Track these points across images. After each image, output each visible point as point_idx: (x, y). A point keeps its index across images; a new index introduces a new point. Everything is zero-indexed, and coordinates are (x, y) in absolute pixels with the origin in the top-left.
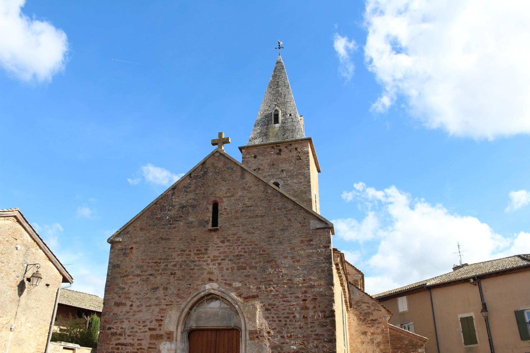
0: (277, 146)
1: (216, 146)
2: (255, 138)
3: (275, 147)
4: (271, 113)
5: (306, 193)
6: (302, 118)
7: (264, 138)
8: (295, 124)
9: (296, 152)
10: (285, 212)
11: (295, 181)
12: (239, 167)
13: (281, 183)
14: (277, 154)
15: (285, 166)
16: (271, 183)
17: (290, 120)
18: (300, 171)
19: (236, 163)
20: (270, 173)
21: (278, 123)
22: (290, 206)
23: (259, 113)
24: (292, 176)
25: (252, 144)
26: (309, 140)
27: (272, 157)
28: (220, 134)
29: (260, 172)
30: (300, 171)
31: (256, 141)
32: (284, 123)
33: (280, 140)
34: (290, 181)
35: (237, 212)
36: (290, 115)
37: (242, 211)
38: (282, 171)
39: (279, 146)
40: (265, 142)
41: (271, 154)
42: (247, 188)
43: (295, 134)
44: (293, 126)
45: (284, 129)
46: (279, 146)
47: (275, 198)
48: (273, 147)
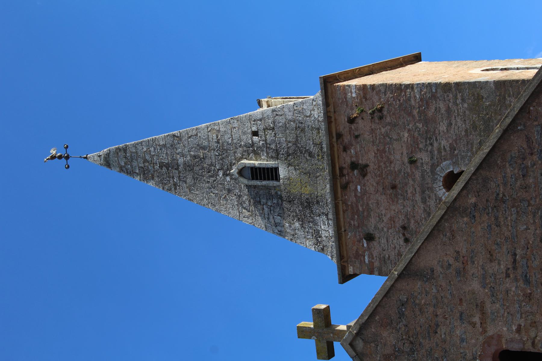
0: (342, 175)
1: (337, 346)
2: (317, 235)
3: (344, 180)
4: (248, 187)
5: (479, 98)
6: (264, 101)
7: (316, 209)
8: (281, 120)
9: (360, 121)
10: (535, 157)
11: (443, 127)
12: (399, 286)
13: (447, 167)
14: (364, 175)
15: (399, 155)
16: (446, 196)
17: (270, 136)
18: (415, 112)
19: (387, 294)
20: (418, 198)
21: (276, 169)
22: (518, 143)
23: (248, 221)
24: (429, 136)
25: (331, 244)
26: (327, 83)
27: (372, 189)
28: (303, 333)
29: (412, 225)
30: (415, 112)
31: (324, 234)
32: (277, 152)
33: (325, 165)
34: (444, 143)
35: (529, 297)
36: (255, 134)
37: (527, 281)
38: (412, 162)
39: (341, 169)
40: (329, 209)
41: (364, 192)
42: (459, 265)
43: (309, 122)
44: (285, 127)
45: (294, 153)
46: (341, 169)
47: (493, 185)
48: (345, 187)
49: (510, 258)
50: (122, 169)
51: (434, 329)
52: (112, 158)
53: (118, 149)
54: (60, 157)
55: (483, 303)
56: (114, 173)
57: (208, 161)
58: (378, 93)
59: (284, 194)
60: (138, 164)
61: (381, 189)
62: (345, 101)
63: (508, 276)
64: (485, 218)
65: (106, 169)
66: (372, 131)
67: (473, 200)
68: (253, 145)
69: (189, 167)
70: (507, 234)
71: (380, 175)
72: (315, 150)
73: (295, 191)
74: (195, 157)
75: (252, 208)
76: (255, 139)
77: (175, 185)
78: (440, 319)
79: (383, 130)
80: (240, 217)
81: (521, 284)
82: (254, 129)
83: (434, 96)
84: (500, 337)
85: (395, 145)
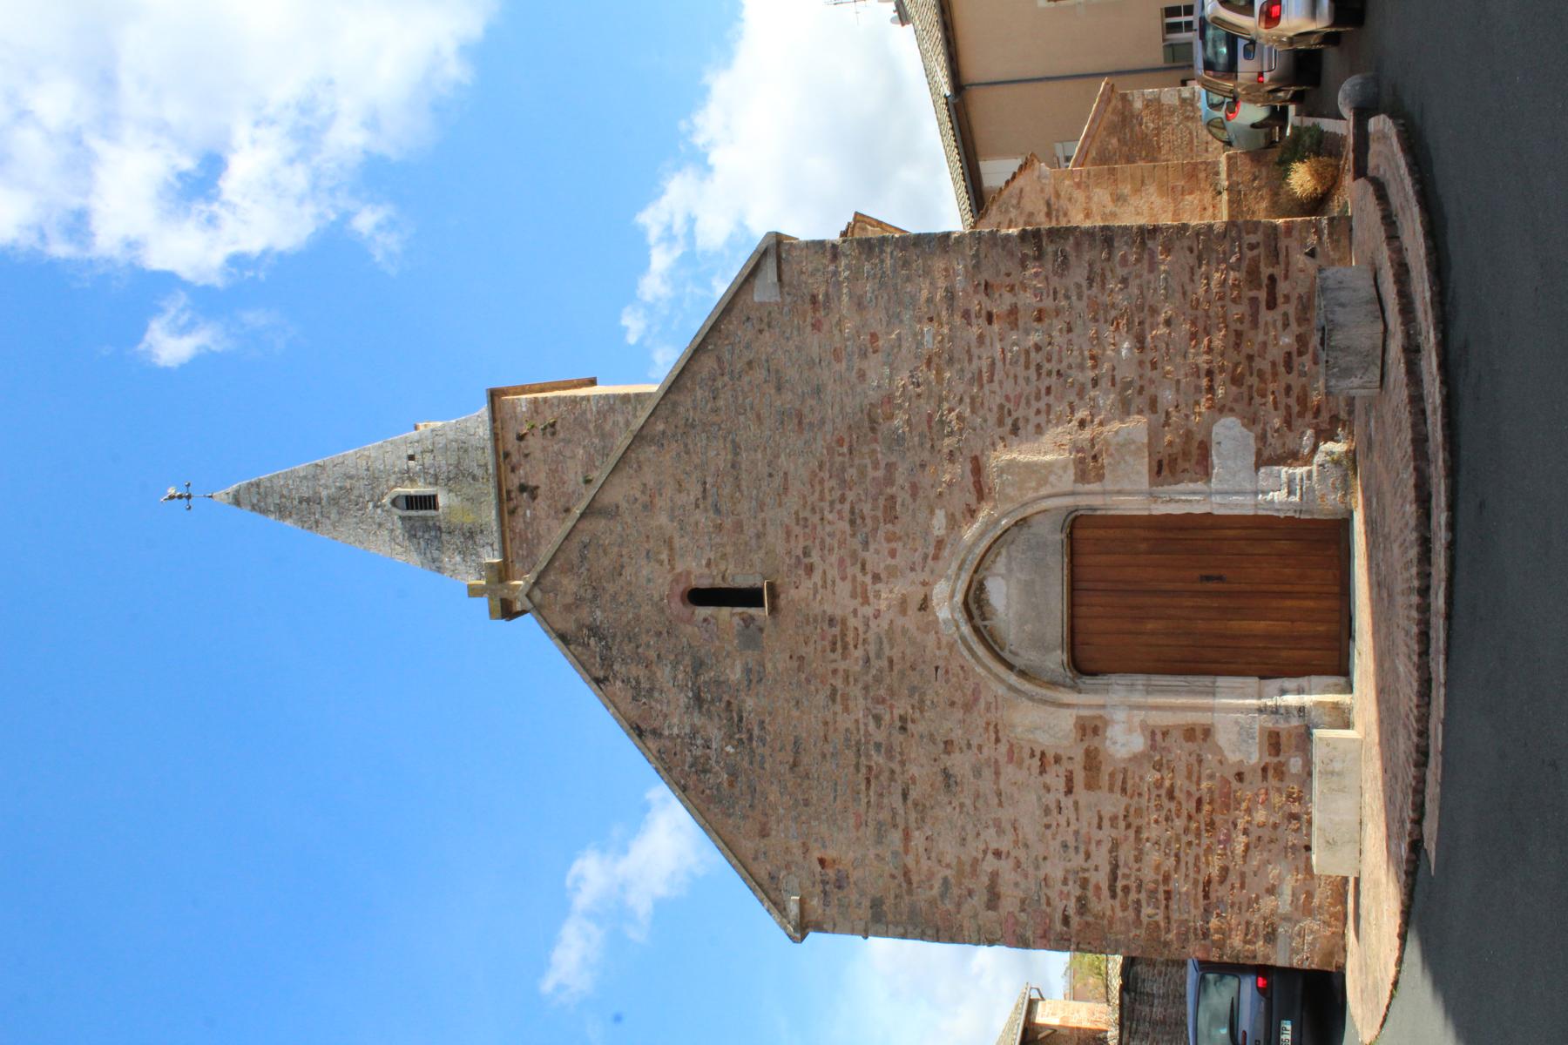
0: (510, 499)
3: (512, 504)
4: (402, 518)
7: (480, 539)
8: (441, 441)
9: (529, 437)
10: (726, 378)
12: (580, 526)
17: (428, 459)
18: (591, 426)
21: (435, 497)
23: (400, 559)
26: (494, 395)
28: (474, 591)
30: (591, 426)
32: (436, 477)
35: (719, 528)
36: (411, 458)
37: (718, 511)
39: (509, 492)
40: (495, 538)
41: (534, 517)
42: (646, 498)
43: (474, 441)
44: (446, 448)
45: (457, 477)
46: (509, 492)
48: (512, 512)
49: (699, 488)
50: (253, 508)
51: (619, 571)
52: (243, 497)
53: (252, 484)
54: (180, 497)
55: (671, 538)
56: (245, 513)
57: (356, 492)
58: (551, 406)
59: (443, 525)
60: (273, 500)
62: (515, 417)
65: (234, 507)
66: (544, 449)
67: (660, 427)
68: (408, 471)
69: (333, 501)
70: (697, 461)
71: (553, 497)
72: (478, 472)
74: (341, 488)
75: (407, 543)
76: (412, 463)
77: (317, 522)
78: (625, 559)
79: (556, 447)
80: (389, 556)
81: (711, 514)
82: (410, 452)
83: (612, 409)
85: (570, 463)
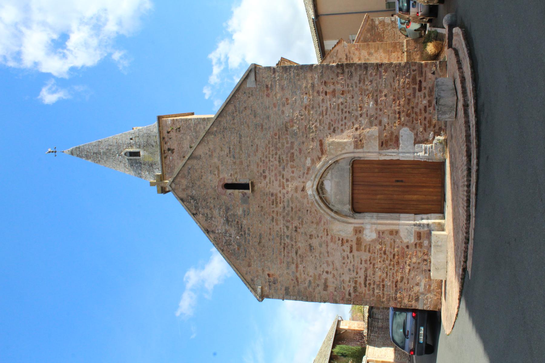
0: (164, 153)
3: (165, 155)
4: (128, 159)
7: (154, 167)
8: (141, 133)
9: (171, 132)
10: (237, 113)
12: (188, 162)
14: (173, 153)
17: (137, 139)
18: (192, 129)
21: (139, 152)
23: (127, 173)
26: (159, 118)
28: (152, 184)
30: (192, 129)
32: (140, 145)
33: (158, 150)
36: (131, 139)
37: (234, 157)
39: (164, 151)
40: (160, 166)
41: (173, 159)
43: (153, 134)
44: (143, 136)
45: (147, 146)
46: (164, 151)
48: (165, 157)
51: (201, 177)
52: (74, 152)
53: (77, 148)
54: (52, 152)
56: (75, 157)
57: (112, 151)
58: (179, 122)
61: (179, 158)
63: (227, 156)
64: (220, 135)
66: (176, 136)
67: (215, 129)
68: (130, 143)
69: (105, 153)
70: (227, 141)
72: (154, 144)
73: (146, 160)
76: (131, 141)
77: (99, 161)
78: (203, 174)
81: (232, 159)
83: (199, 123)
84: (224, 178)
85: (185, 141)
